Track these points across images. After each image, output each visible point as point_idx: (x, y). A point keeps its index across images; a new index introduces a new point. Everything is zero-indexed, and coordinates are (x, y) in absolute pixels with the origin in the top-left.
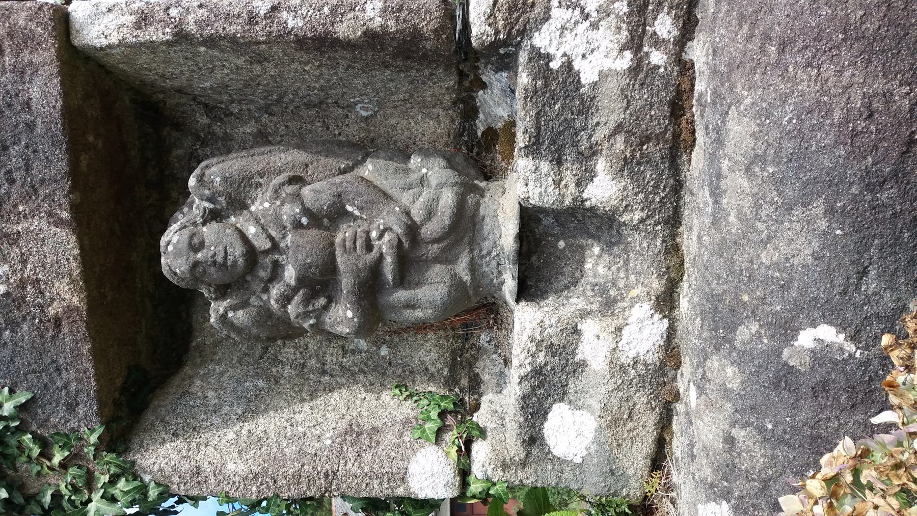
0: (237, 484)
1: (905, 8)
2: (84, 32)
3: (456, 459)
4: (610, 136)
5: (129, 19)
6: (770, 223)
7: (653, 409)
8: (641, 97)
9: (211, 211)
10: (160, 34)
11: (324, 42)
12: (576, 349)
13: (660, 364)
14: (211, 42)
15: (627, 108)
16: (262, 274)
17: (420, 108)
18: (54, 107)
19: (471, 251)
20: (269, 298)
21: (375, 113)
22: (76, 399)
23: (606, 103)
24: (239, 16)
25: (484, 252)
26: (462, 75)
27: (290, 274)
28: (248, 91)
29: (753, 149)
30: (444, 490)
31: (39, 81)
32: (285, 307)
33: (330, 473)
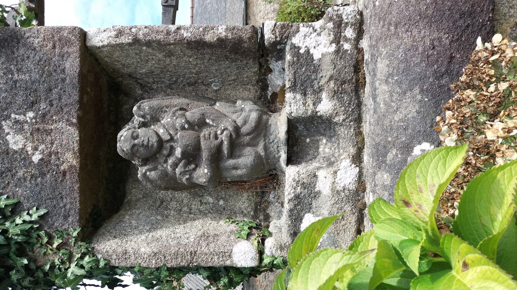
0: (145, 259)
1: (443, 3)
2: (92, 40)
3: (257, 246)
4: (328, 82)
5: (114, 33)
6: (397, 102)
7: (354, 214)
8: (340, 64)
9: (143, 122)
10: (127, 39)
11: (200, 43)
12: (315, 185)
13: (356, 190)
14: (149, 44)
15: (334, 69)
16: (165, 152)
17: (241, 85)
18: (76, 71)
19: (265, 140)
20: (167, 166)
21: (221, 88)
22: (69, 213)
23: (325, 67)
24: (162, 32)
25: (271, 141)
26: (261, 66)
28: (162, 75)
29: (388, 72)
30: (250, 262)
31: (70, 60)
32: (174, 170)
33: (193, 252)
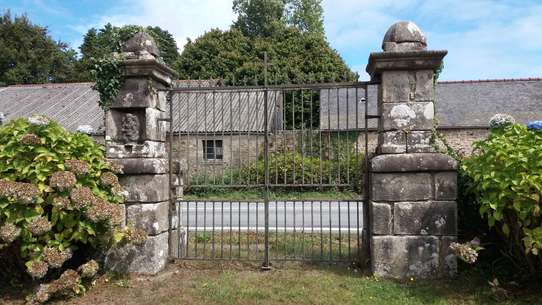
27: (127, 125)
